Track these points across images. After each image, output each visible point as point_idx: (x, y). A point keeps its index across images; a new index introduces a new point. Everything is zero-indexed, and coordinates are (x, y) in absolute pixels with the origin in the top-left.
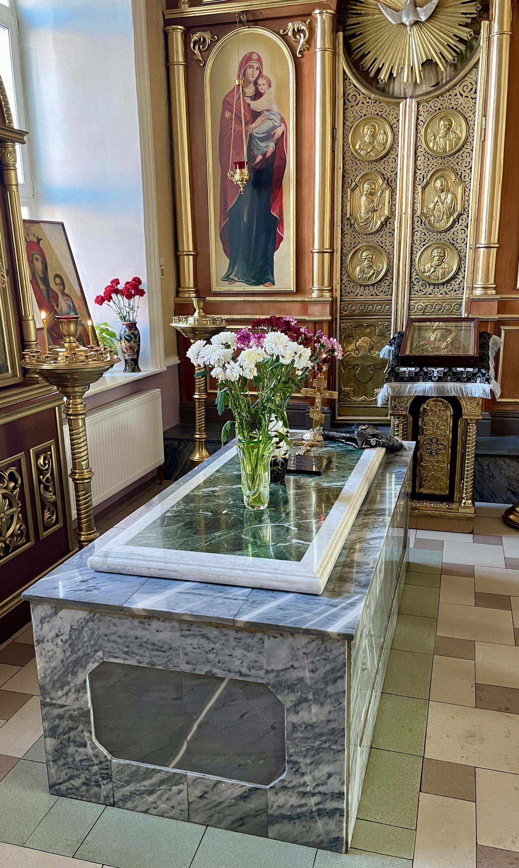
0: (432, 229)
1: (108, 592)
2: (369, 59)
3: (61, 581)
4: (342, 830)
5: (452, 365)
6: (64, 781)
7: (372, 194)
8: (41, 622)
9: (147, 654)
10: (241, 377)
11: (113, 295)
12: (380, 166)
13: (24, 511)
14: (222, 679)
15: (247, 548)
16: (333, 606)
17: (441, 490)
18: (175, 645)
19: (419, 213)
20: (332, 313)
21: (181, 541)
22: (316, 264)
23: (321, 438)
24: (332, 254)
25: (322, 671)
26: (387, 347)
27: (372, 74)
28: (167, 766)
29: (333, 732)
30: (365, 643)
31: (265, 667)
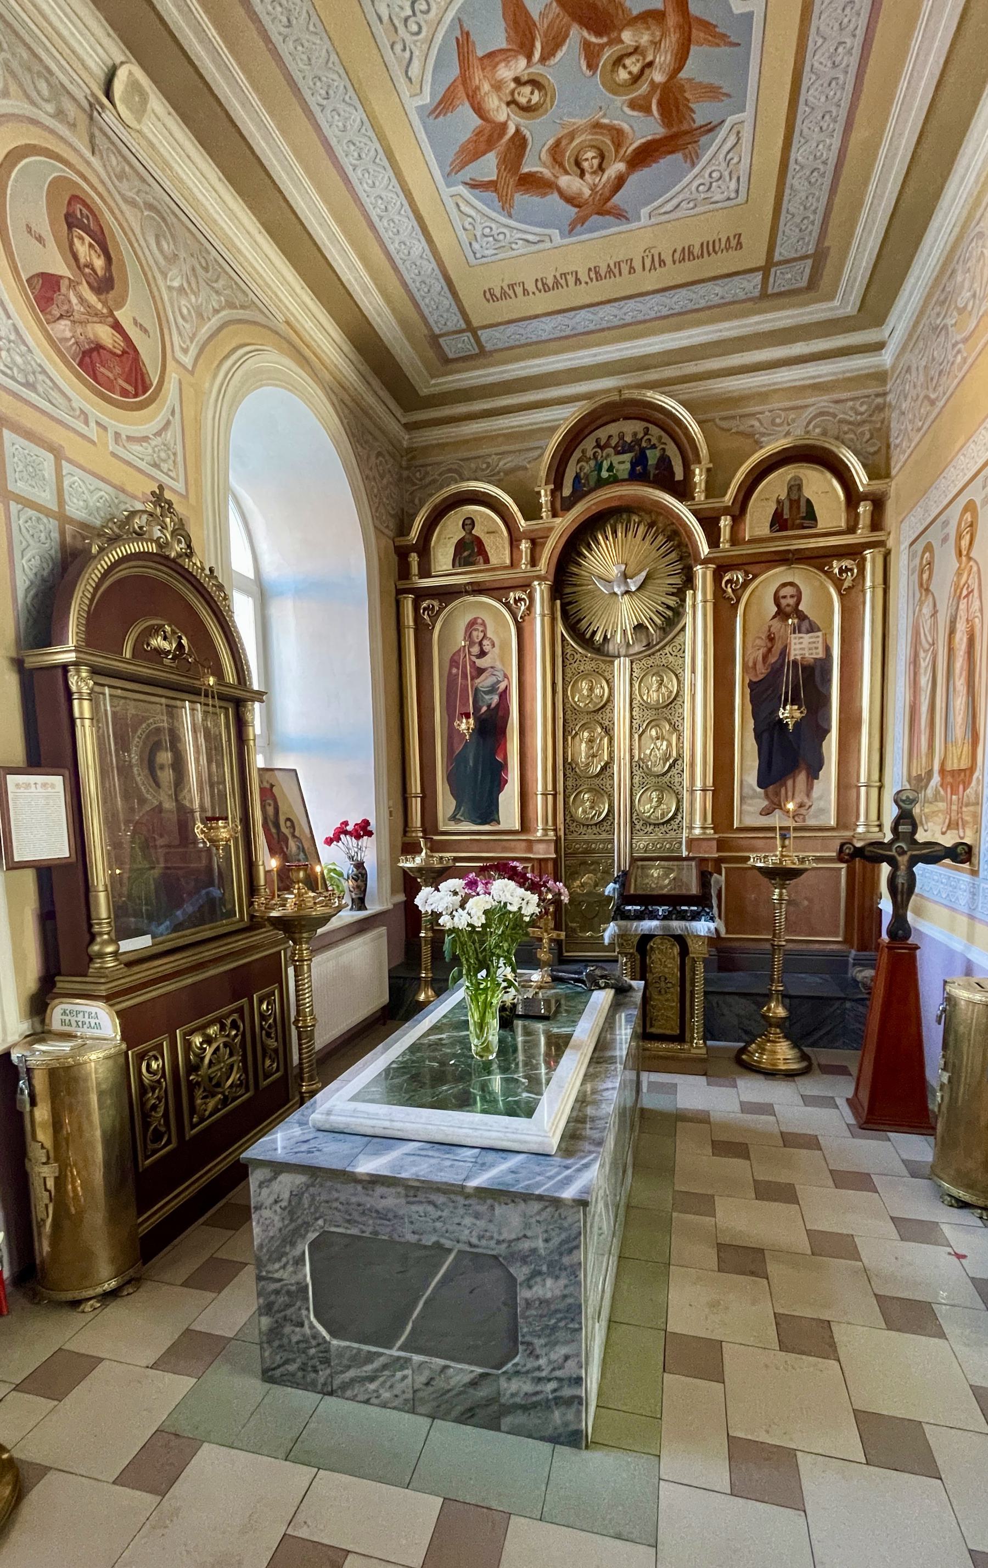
0: (649, 773)
1: (330, 1155)
2: (584, 624)
3: (280, 1141)
4: (581, 1421)
5: (677, 904)
6: (279, 1366)
7: (591, 741)
8: (260, 1186)
9: (371, 1222)
10: (469, 925)
11: (342, 836)
12: (598, 717)
13: (244, 1060)
14: (449, 1251)
15: (475, 1103)
16: (567, 1167)
17: (672, 1029)
18: (401, 1213)
19: (636, 758)
20: (557, 851)
21: (407, 1096)
22: (539, 804)
23: (549, 979)
24: (555, 796)
25: (556, 1241)
26: (612, 885)
27: (588, 636)
28: (390, 1348)
29: (569, 1309)
30: (601, 1205)
31: (496, 1236)
